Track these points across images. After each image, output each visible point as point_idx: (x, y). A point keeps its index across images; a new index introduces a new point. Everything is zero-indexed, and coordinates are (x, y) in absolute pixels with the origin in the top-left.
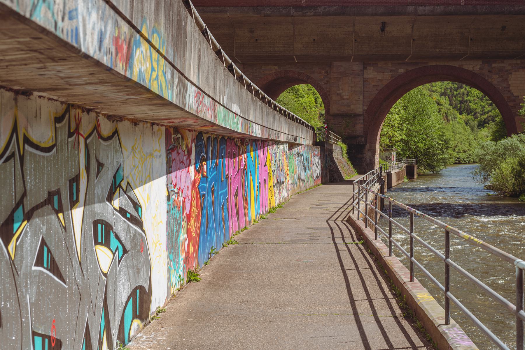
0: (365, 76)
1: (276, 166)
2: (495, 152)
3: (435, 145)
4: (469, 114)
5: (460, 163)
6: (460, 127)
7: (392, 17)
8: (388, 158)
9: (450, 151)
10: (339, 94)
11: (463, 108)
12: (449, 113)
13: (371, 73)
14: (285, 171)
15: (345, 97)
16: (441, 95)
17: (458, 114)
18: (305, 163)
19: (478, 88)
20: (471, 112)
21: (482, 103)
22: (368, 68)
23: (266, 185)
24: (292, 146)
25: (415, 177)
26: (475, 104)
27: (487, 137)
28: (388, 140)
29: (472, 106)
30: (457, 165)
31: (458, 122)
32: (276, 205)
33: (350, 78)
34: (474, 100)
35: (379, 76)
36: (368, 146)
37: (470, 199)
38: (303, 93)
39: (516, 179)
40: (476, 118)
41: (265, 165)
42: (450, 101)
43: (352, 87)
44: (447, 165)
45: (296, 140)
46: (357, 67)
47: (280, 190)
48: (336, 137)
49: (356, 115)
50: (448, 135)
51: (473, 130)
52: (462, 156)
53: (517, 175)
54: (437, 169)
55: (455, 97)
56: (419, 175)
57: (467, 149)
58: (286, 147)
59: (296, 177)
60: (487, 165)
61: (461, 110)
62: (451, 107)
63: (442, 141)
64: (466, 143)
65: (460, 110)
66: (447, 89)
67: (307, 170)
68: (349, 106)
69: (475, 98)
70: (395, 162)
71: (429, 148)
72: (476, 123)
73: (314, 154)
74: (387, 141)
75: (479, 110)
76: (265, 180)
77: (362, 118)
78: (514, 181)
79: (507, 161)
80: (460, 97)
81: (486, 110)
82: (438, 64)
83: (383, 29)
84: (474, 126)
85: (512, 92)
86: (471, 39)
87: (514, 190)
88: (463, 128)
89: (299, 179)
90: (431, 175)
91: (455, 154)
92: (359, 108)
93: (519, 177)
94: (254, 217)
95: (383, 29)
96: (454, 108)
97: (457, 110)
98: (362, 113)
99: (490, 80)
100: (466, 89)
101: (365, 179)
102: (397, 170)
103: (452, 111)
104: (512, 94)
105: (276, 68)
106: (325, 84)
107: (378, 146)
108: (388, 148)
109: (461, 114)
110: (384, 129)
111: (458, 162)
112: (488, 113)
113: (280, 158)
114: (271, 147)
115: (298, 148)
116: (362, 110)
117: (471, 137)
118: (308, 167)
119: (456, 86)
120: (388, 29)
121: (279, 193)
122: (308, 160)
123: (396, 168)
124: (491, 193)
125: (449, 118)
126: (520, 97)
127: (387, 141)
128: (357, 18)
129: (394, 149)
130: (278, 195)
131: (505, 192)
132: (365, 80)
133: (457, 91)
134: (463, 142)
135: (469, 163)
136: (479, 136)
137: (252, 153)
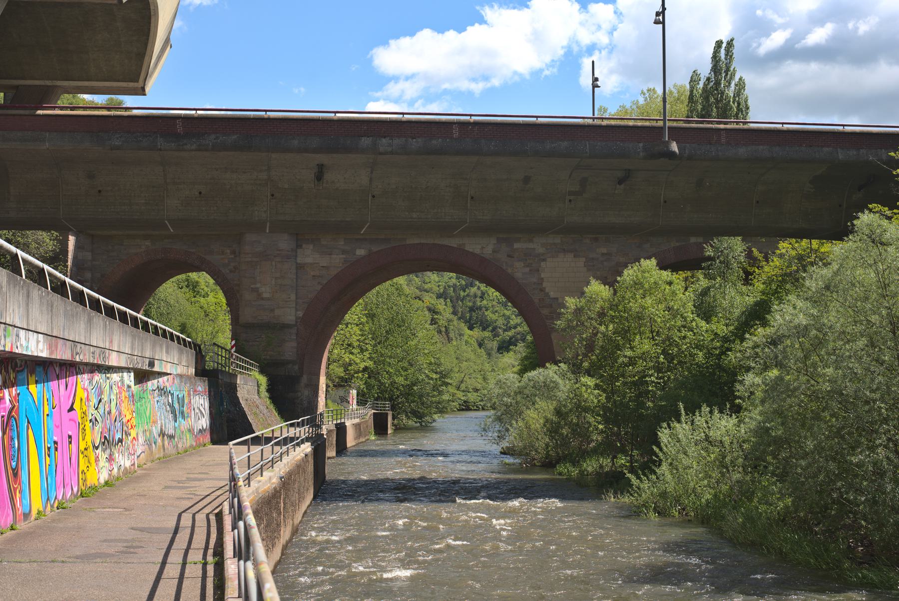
0: (299, 260)
1: (101, 410)
2: (520, 392)
3: (423, 380)
4: (484, 329)
5: (468, 409)
6: (470, 349)
7: (334, 155)
8: (344, 400)
9: (452, 390)
10: (256, 290)
11: (474, 319)
12: (452, 327)
13: (309, 256)
14: (125, 420)
15: (265, 295)
16: (439, 296)
17: (466, 329)
18: (176, 405)
19: (497, 289)
20: (488, 326)
21: (505, 311)
22: (304, 246)
23: (73, 447)
24: (142, 376)
25: (390, 431)
26: (494, 312)
27: (514, 367)
28: (342, 369)
29: (490, 315)
30: (464, 413)
31: (467, 342)
32: (102, 481)
33: (274, 263)
34: (493, 306)
35: (322, 261)
36: (304, 379)
37: (481, 471)
38: (206, 289)
39: (552, 438)
40: (496, 335)
41: (71, 409)
42: (454, 307)
43: (276, 278)
44: (447, 413)
45: (152, 364)
46: (284, 243)
47: (111, 455)
48: (246, 362)
49: (284, 327)
50: (447, 362)
51: (489, 355)
52: (472, 397)
53: (553, 430)
54: (428, 418)
55: (462, 301)
56: (398, 429)
57: (479, 386)
58: (129, 378)
59: (156, 431)
60: (507, 413)
61: (472, 322)
62: (455, 318)
63: (436, 373)
64: (478, 376)
65: (469, 322)
66: (449, 286)
67: (180, 419)
68: (272, 310)
69: (494, 303)
70: (355, 407)
71: (414, 384)
72: (495, 344)
73: (195, 391)
74: (340, 371)
75: (501, 322)
76: (70, 437)
77: (294, 331)
78: (547, 440)
79: (537, 406)
80: (470, 301)
81: (512, 322)
82: (423, 241)
83: (319, 177)
84: (492, 349)
85: (547, 290)
86: (472, 198)
87: (548, 455)
88: (474, 351)
89: (162, 434)
90: (416, 428)
91: (460, 394)
92: (290, 315)
93: (556, 432)
94: (37, 505)
95: (319, 177)
96: (459, 319)
97: (466, 322)
98: (294, 323)
99: (510, 271)
100: (479, 288)
101: (298, 435)
102: (357, 421)
103: (455, 322)
104: (547, 295)
105: (148, 243)
106: (231, 271)
107: (323, 380)
108: (341, 384)
109: (471, 328)
110: (332, 349)
111: (466, 407)
112: (515, 327)
113: (113, 397)
114: (86, 376)
115: (160, 380)
116: (294, 318)
117: (487, 367)
118: (183, 413)
119: (464, 283)
120: (328, 176)
121: (110, 459)
122: (181, 401)
123: (356, 417)
124: (509, 460)
125: (452, 335)
126: (560, 300)
127: (340, 371)
128: (274, 156)
129: (353, 385)
130: (107, 464)
131: (534, 459)
132: (300, 267)
133: (464, 291)
134: (474, 375)
135: (483, 409)
136: (500, 365)
137: (32, 387)
